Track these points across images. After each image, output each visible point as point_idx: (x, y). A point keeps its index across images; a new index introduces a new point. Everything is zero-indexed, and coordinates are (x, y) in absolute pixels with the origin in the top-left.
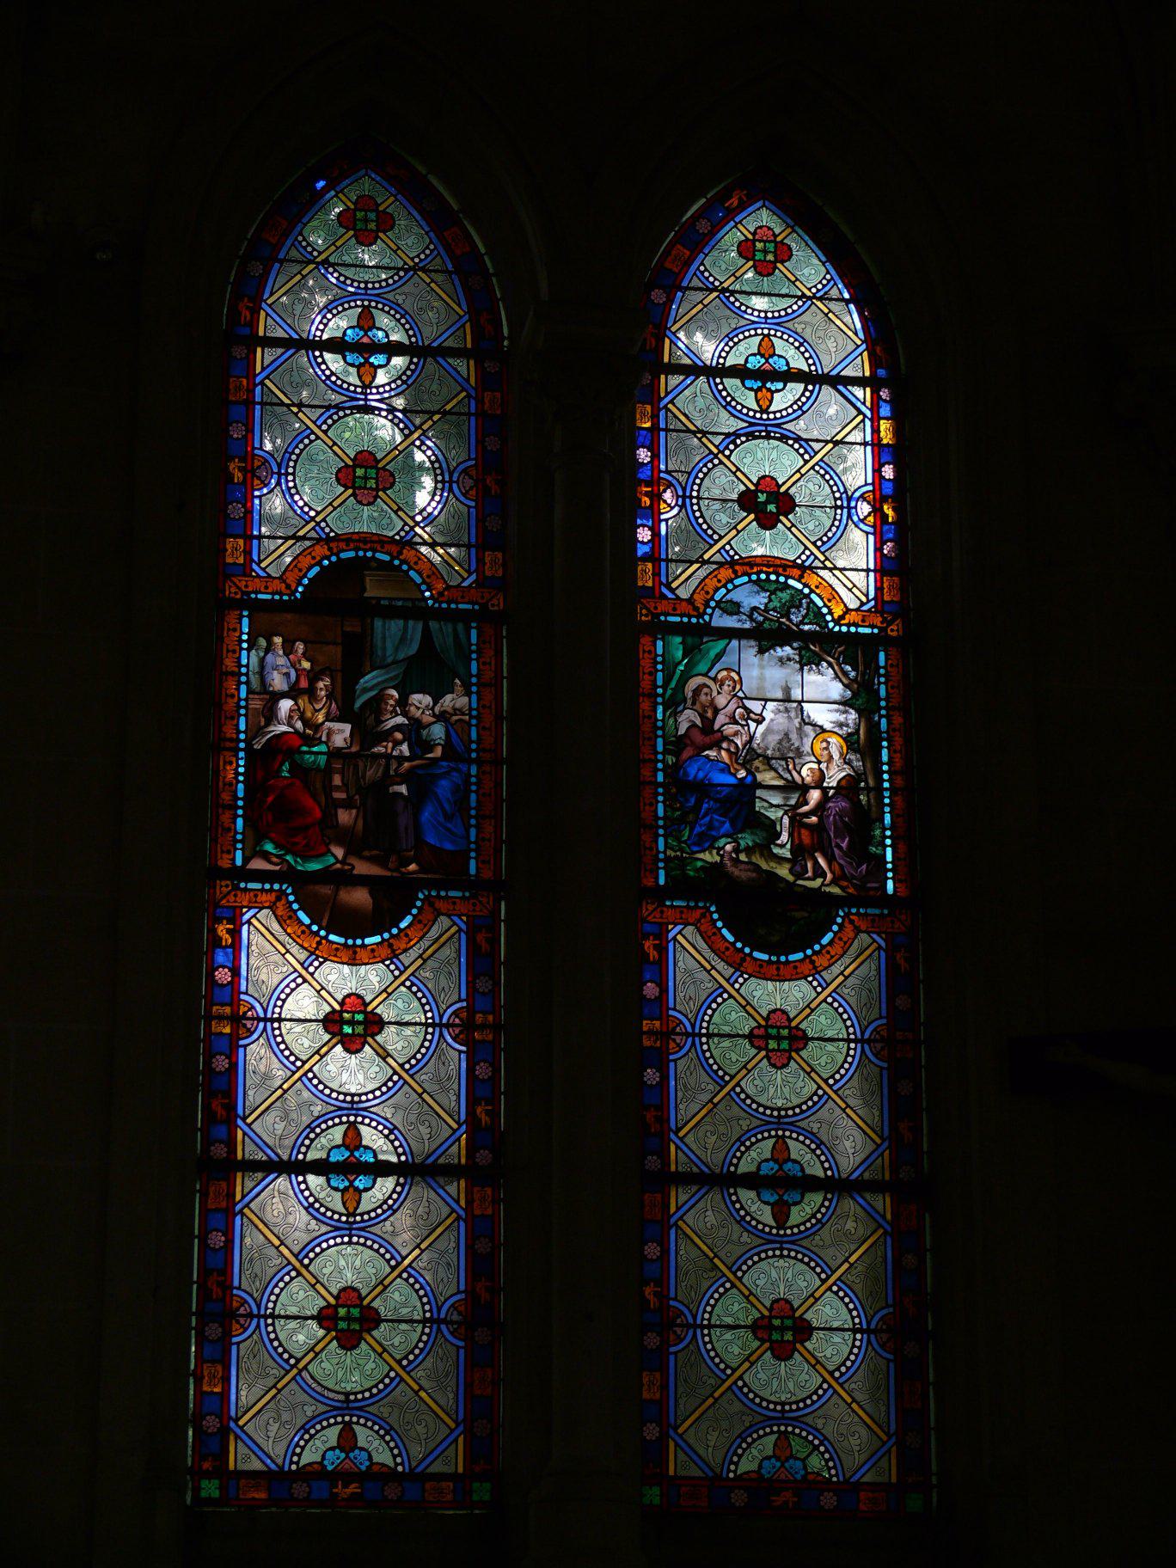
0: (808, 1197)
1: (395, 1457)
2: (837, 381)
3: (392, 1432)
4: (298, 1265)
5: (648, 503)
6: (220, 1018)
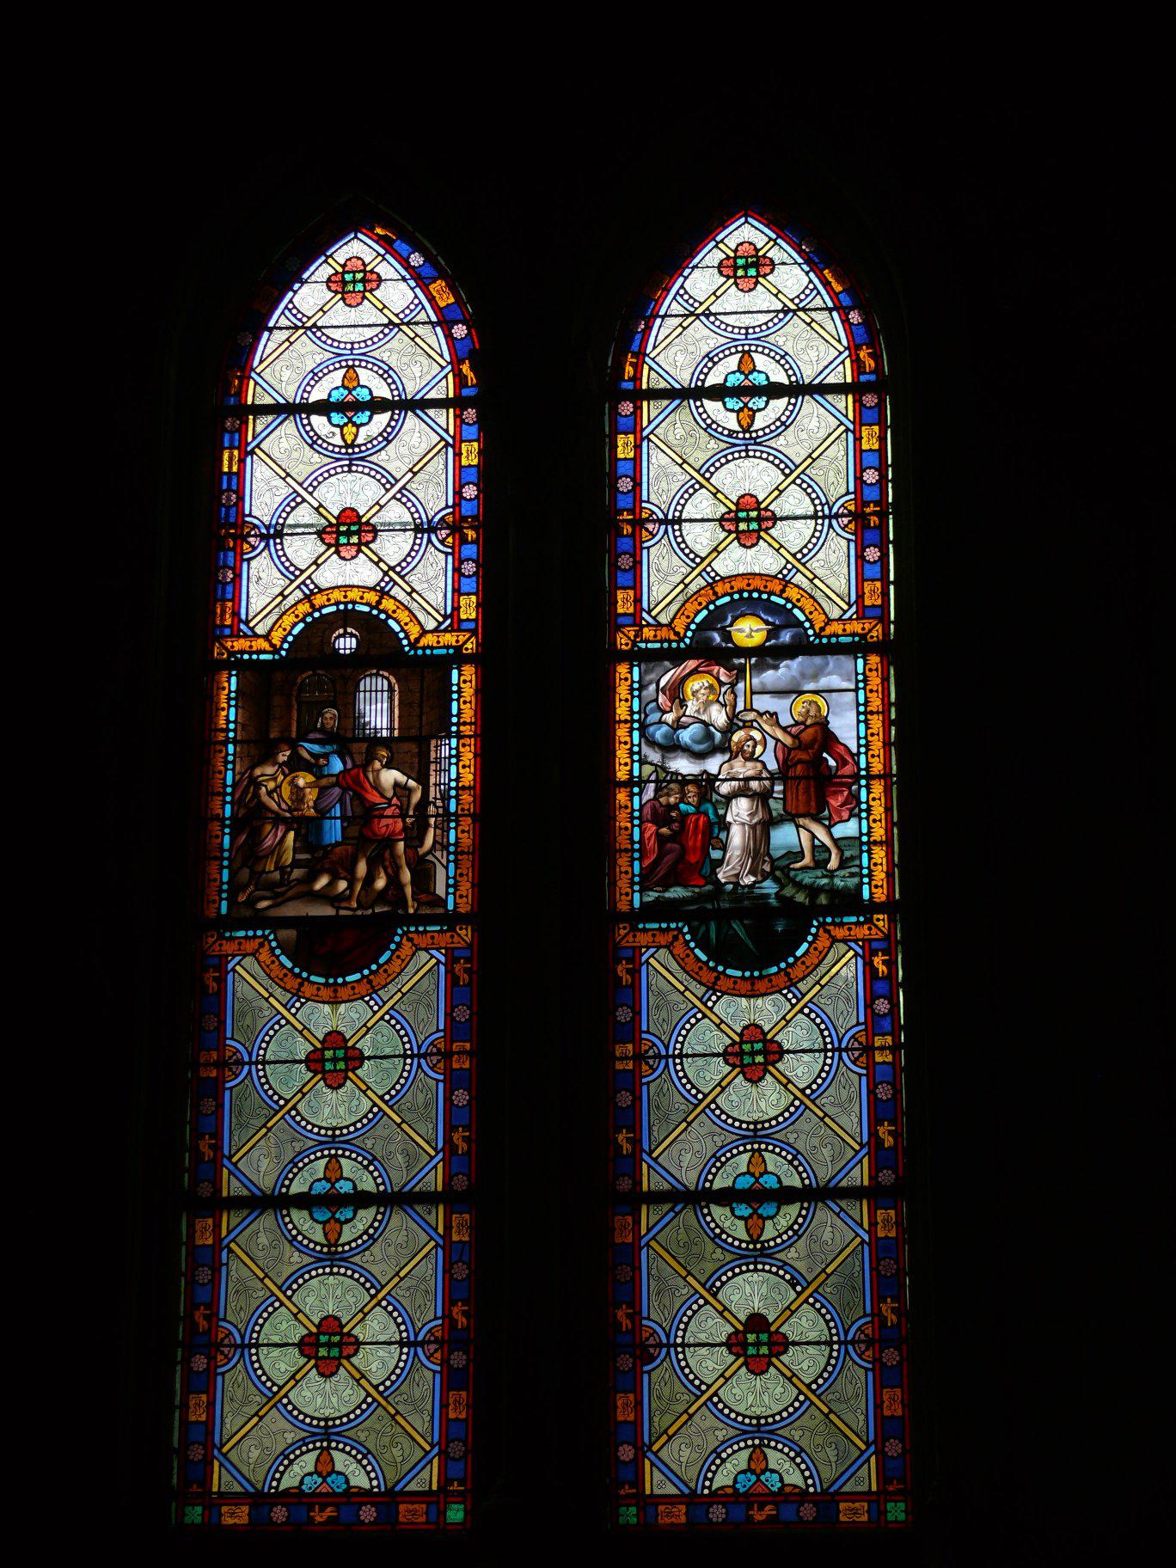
0: (785, 1209)
1: (806, 1479)
2: (418, 405)
3: (370, 1456)
4: (380, 1296)
5: (630, 530)
6: (207, 1065)
